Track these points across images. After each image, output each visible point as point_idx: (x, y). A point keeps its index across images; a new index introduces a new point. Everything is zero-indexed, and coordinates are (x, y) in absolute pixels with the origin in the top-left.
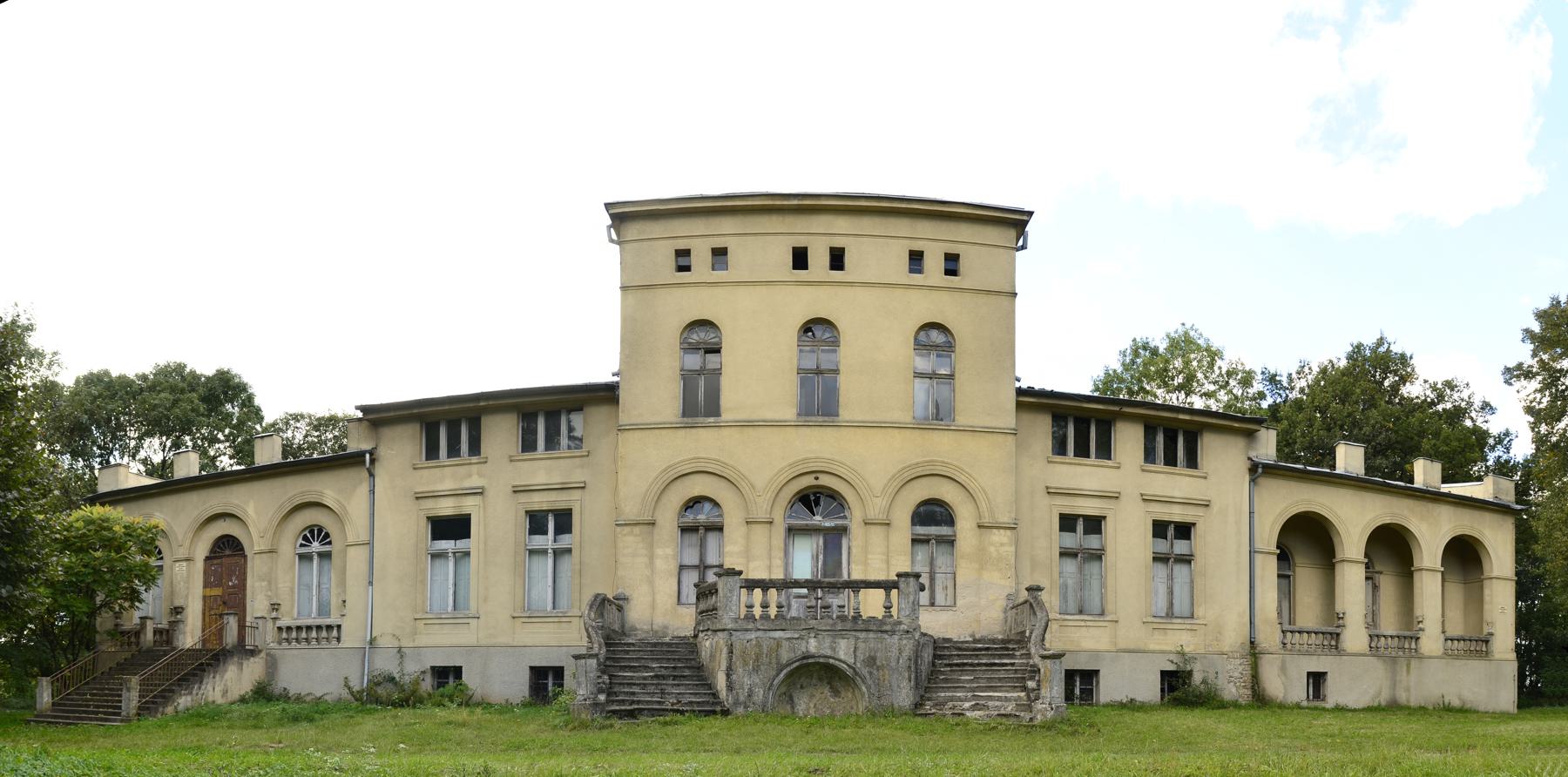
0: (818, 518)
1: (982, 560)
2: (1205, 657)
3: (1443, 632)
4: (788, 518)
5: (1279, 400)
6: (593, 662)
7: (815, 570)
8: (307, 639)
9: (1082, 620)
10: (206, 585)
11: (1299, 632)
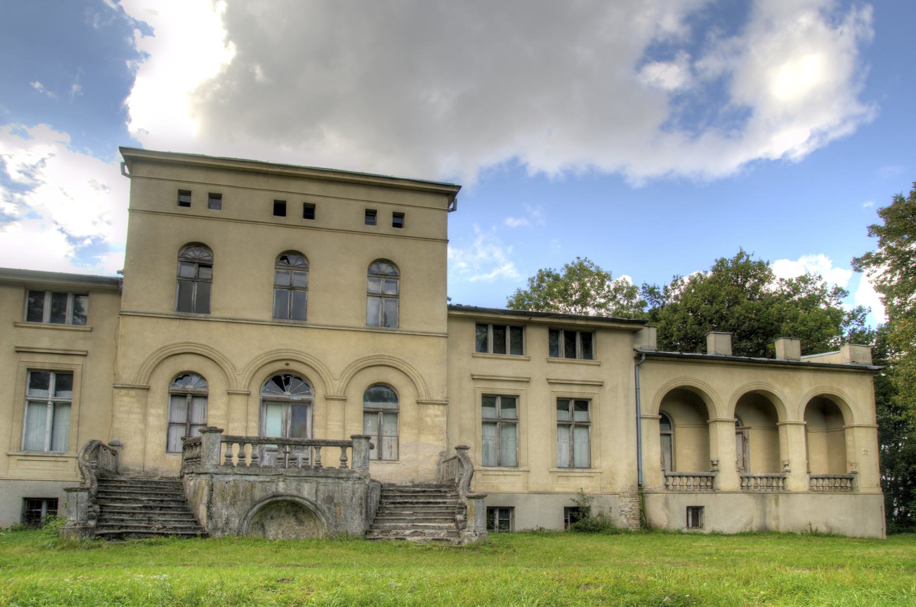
1: (420, 426)
2: (600, 497)
3: (809, 472)
4: (263, 392)
5: (657, 306)
6: (85, 495)
7: (284, 431)
9: (501, 471)
11: (679, 477)
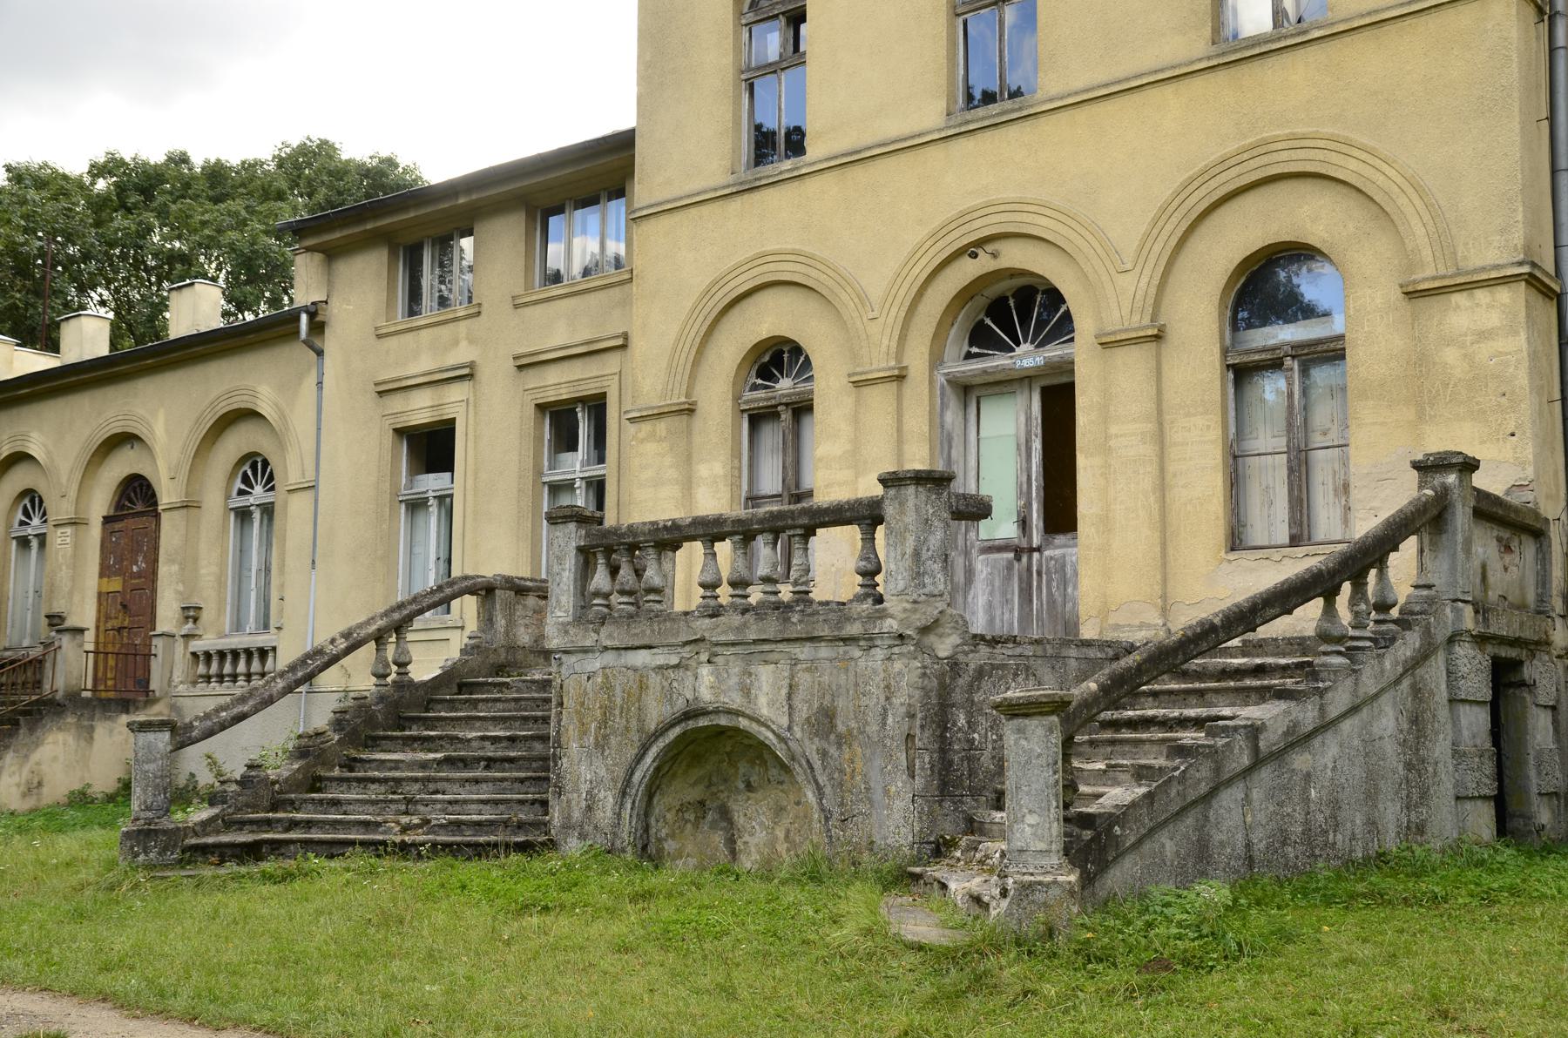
7: (1025, 479)
10: (105, 571)
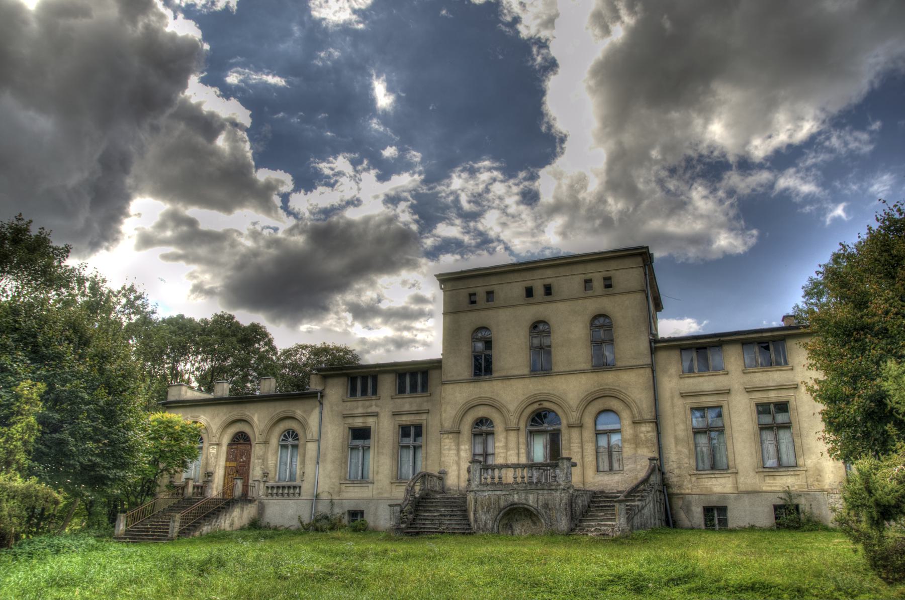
0: (546, 425)
8: (294, 494)
10: (228, 460)
